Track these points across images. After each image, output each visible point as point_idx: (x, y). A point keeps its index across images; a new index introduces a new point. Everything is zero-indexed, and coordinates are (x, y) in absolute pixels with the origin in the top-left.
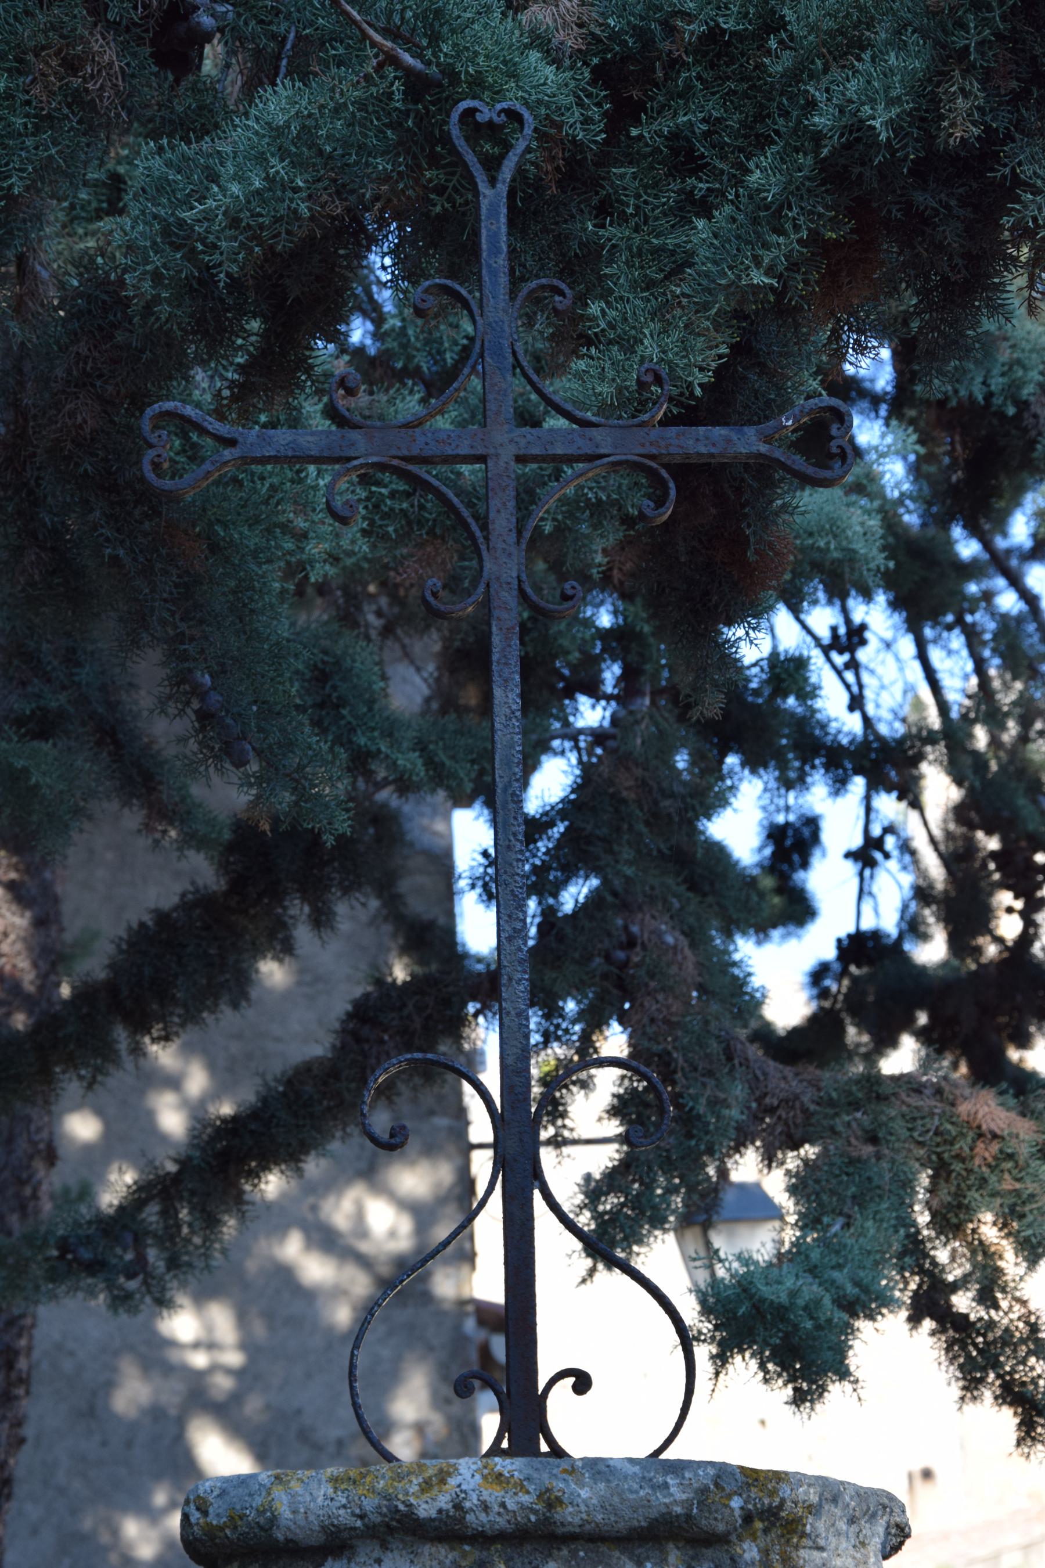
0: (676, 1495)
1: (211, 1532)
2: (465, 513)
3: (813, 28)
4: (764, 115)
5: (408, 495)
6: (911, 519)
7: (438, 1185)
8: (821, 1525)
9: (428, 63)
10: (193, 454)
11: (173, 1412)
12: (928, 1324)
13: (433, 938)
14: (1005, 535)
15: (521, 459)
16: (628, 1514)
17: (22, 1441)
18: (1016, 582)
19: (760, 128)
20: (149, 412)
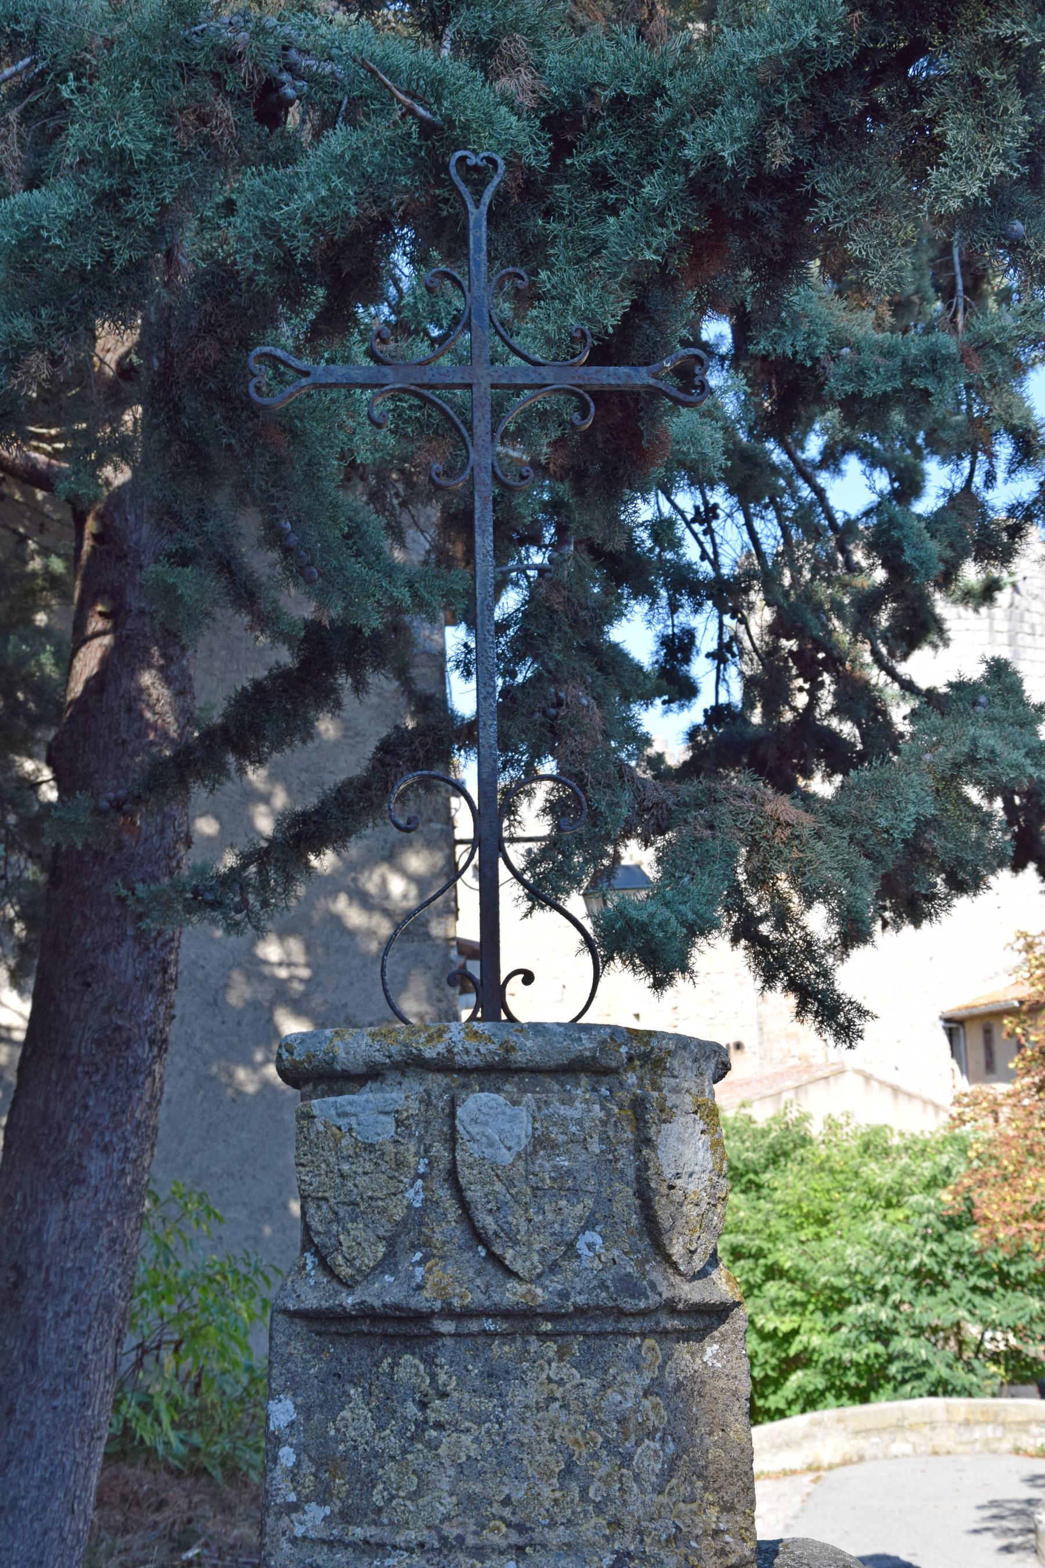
0: (587, 1046)
1: (295, 1065)
2: (458, 421)
3: (684, 93)
4: (652, 151)
5: (421, 408)
6: (743, 436)
7: (434, 866)
8: (676, 1063)
9: (434, 114)
10: (280, 378)
11: (266, 1004)
12: (743, 942)
13: (433, 704)
14: (803, 449)
15: (493, 386)
16: (556, 1056)
17: (173, 1017)
18: (810, 480)
19: (650, 159)
20: (253, 354)
